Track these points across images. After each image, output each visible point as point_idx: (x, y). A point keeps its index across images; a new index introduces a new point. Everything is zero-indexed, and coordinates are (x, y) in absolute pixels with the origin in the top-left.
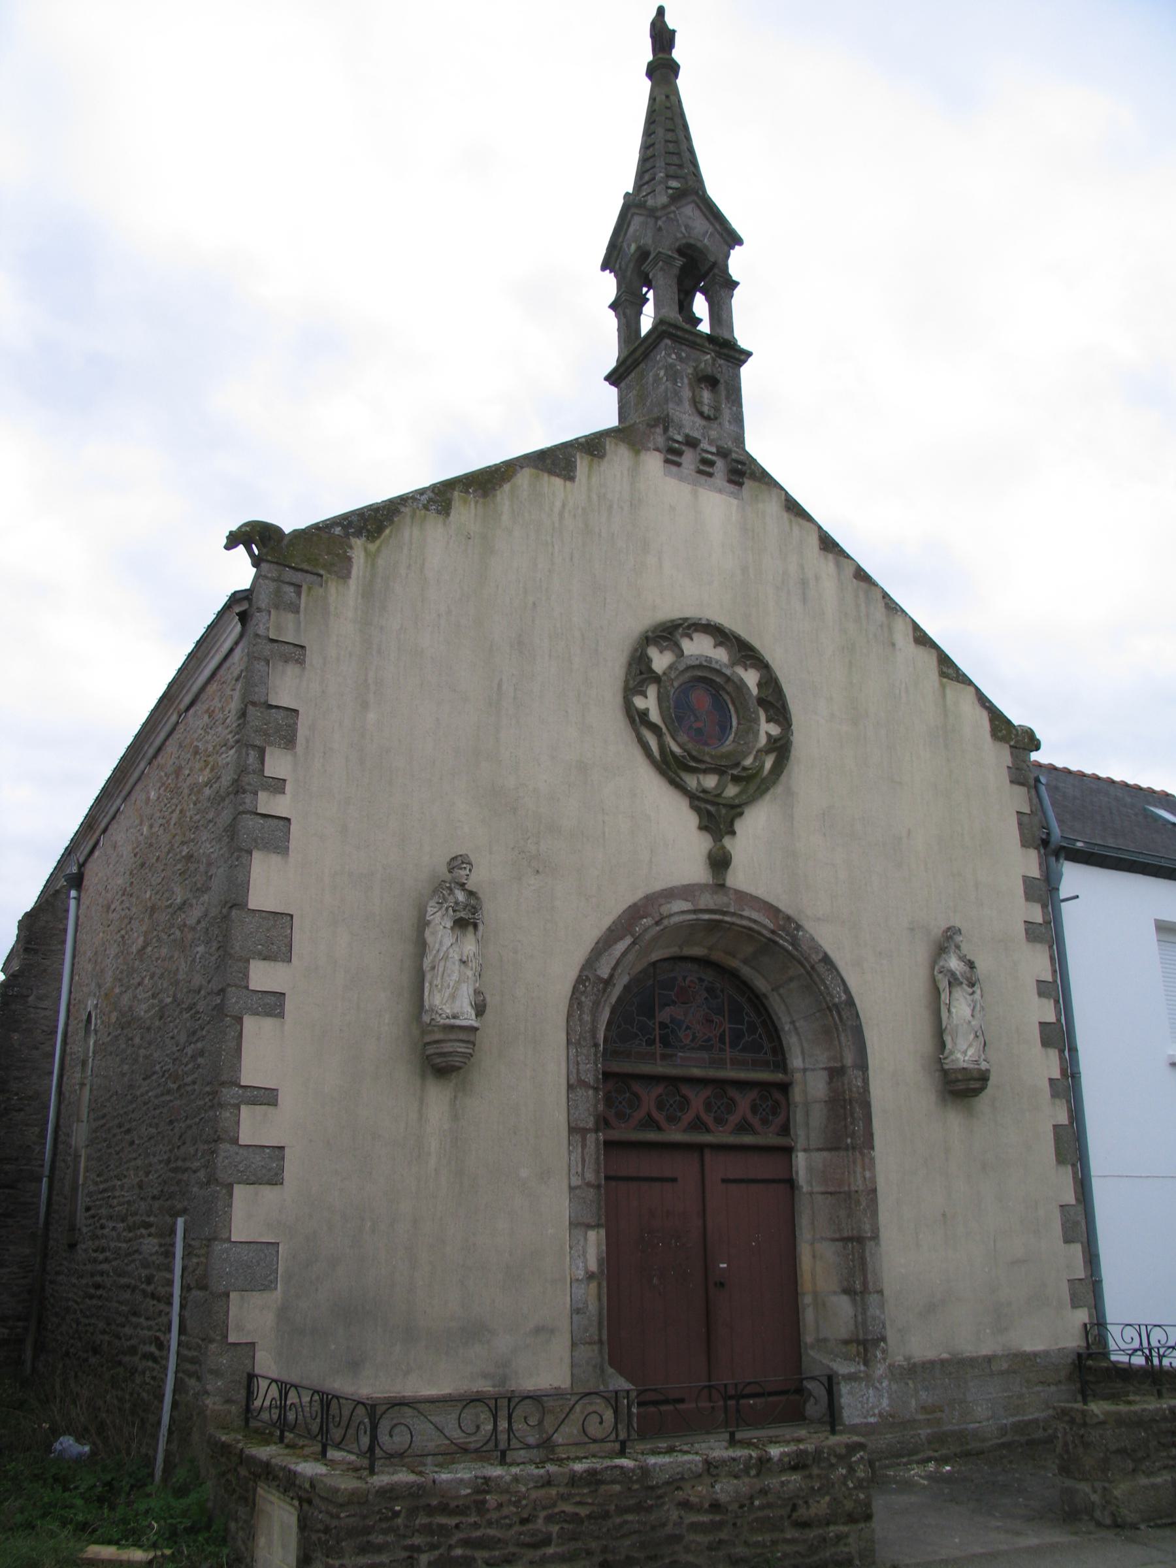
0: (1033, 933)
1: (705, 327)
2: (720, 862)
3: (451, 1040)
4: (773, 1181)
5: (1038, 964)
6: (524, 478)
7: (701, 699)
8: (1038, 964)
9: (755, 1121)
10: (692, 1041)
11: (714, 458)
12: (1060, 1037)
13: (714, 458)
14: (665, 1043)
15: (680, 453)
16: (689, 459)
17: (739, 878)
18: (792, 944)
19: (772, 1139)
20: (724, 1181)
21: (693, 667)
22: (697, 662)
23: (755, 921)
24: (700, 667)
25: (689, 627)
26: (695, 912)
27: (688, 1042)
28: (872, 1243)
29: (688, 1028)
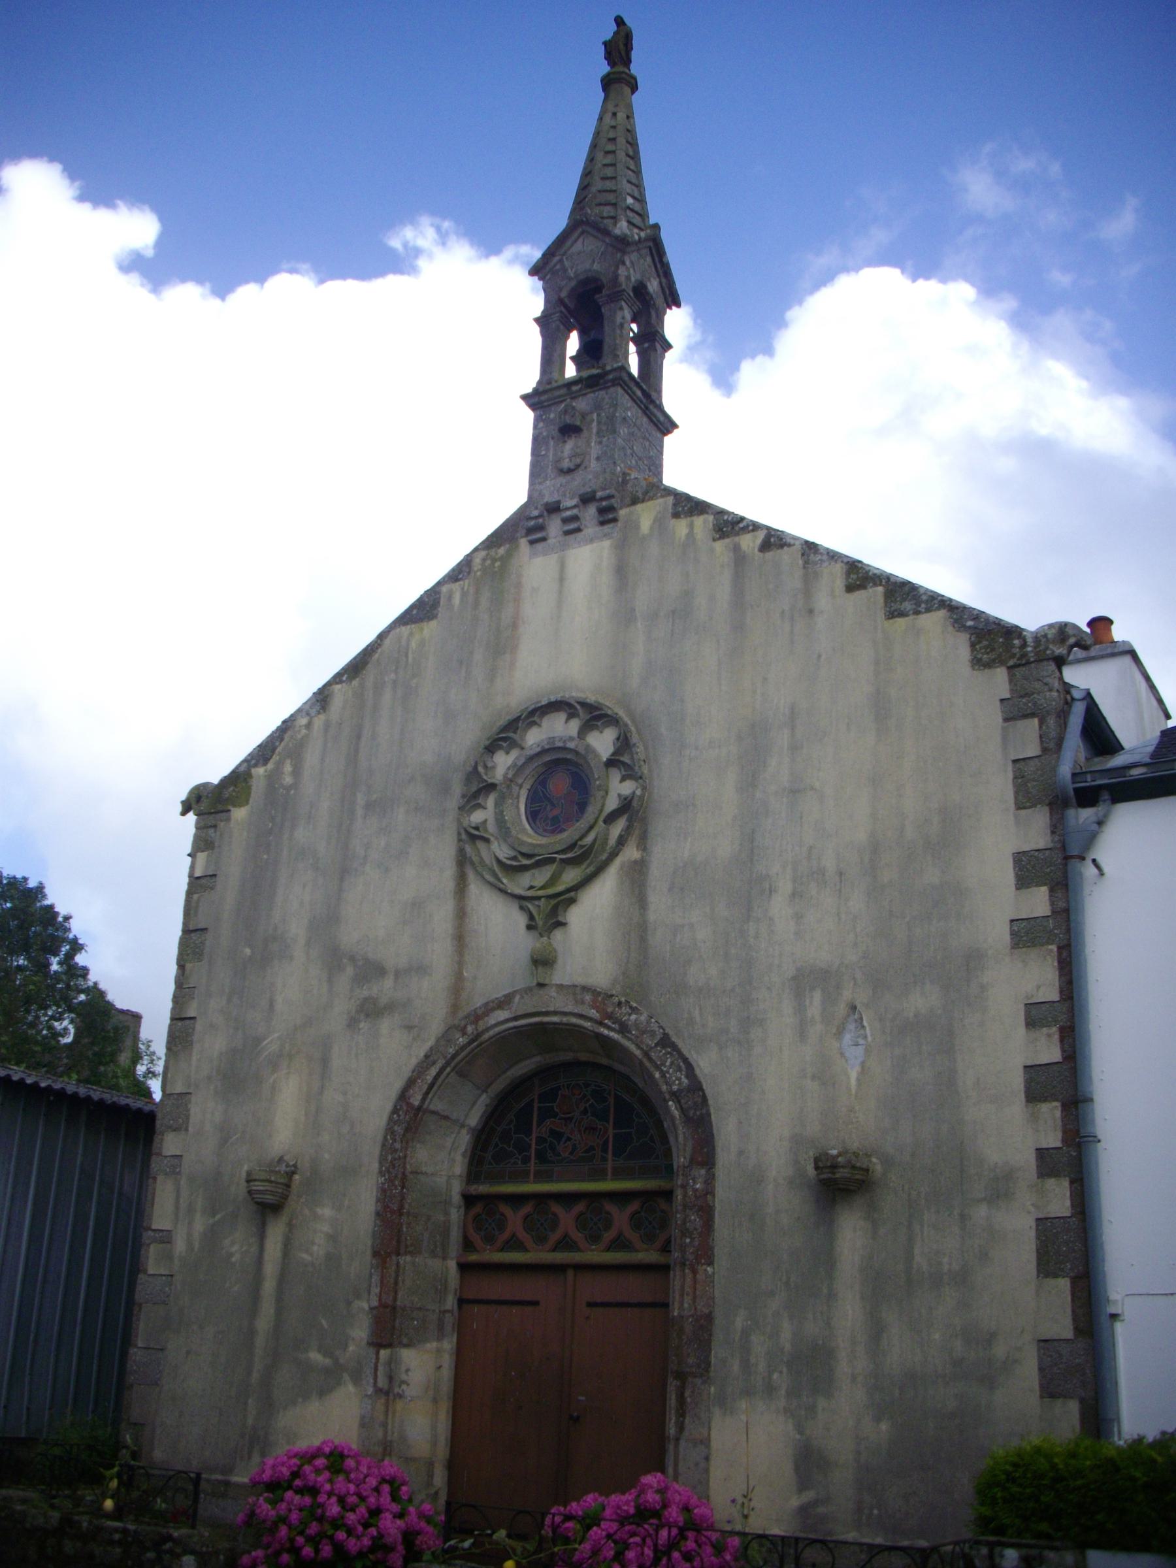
0: (1025, 934)
1: (634, 369)
2: (542, 961)
3: (178, 1191)
4: (639, 1305)
5: (1039, 978)
6: (933, 621)
7: (560, 784)
8: (1039, 978)
9: (577, 1236)
10: (571, 1153)
11: (575, 511)
12: (1063, 1085)
13: (575, 511)
14: (541, 1157)
15: (541, 528)
16: (554, 527)
17: (568, 971)
18: (620, 1032)
19: (647, 1255)
20: (590, 1305)
21: (538, 754)
22: (539, 749)
23: (581, 1016)
24: (544, 752)
25: (528, 717)
26: (516, 1018)
27: (567, 1154)
28: (698, 1381)
29: (569, 1139)
